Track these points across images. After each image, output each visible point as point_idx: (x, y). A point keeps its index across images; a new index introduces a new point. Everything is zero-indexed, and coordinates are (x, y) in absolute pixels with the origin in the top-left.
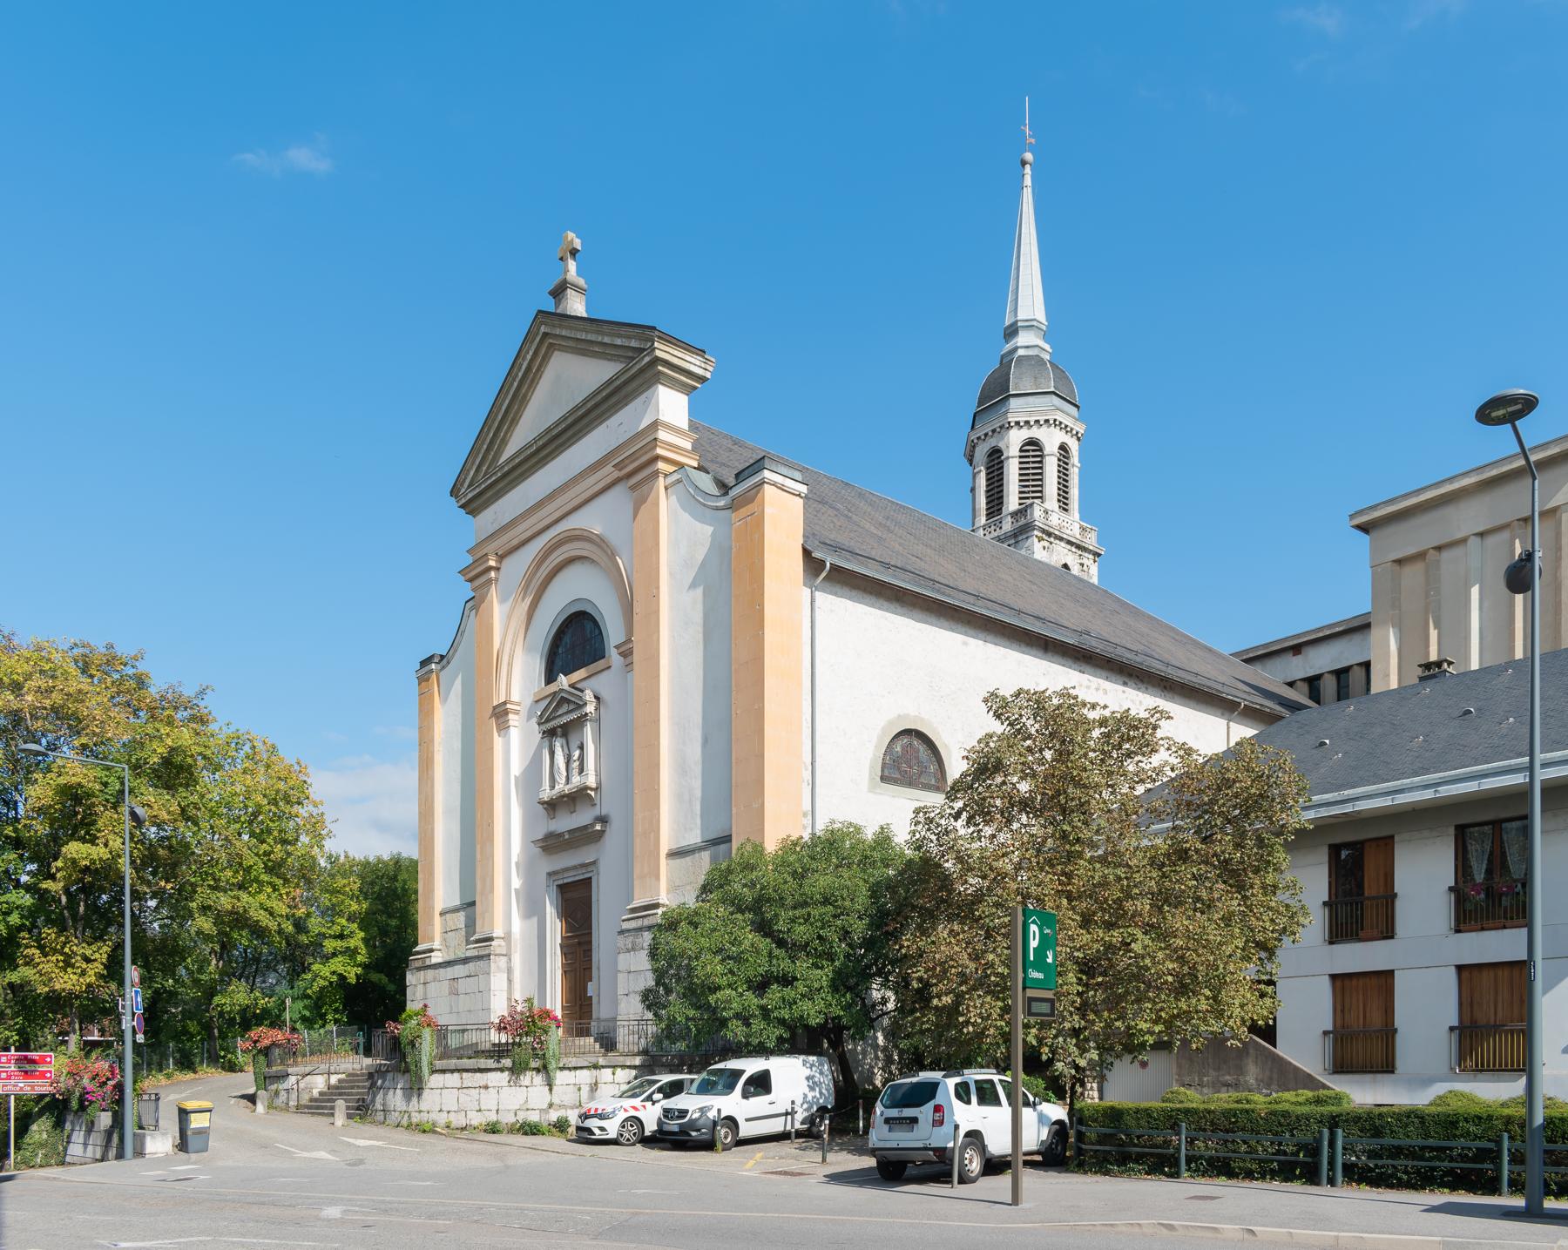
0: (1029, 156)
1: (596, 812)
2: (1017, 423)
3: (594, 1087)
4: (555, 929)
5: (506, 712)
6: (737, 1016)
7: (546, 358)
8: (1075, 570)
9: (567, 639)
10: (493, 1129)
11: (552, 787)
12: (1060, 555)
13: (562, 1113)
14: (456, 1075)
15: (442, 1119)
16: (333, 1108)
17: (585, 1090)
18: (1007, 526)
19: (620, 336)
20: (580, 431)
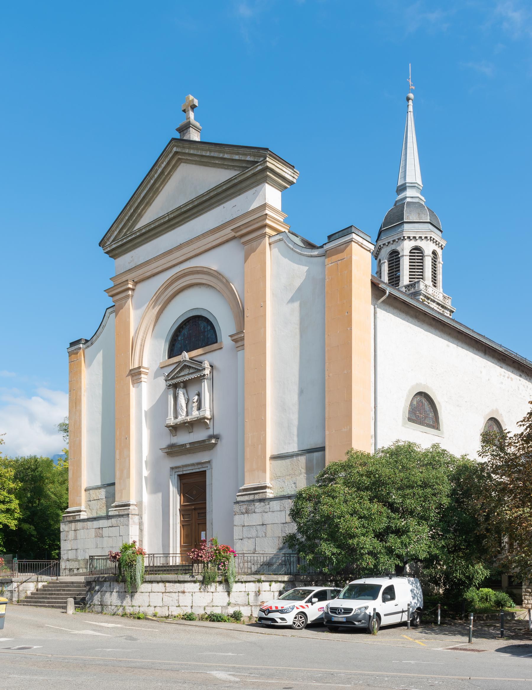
0: (411, 96)
1: (210, 432)
2: (409, 237)
3: (258, 593)
4: (175, 500)
5: (140, 373)
6: (370, 553)
7: (175, 167)
9: (185, 331)
10: (189, 617)
11: (176, 417)
13: (236, 609)
14: (161, 585)
15: (150, 611)
16: (66, 603)
17: (252, 595)
19: (238, 154)
20: (203, 209)
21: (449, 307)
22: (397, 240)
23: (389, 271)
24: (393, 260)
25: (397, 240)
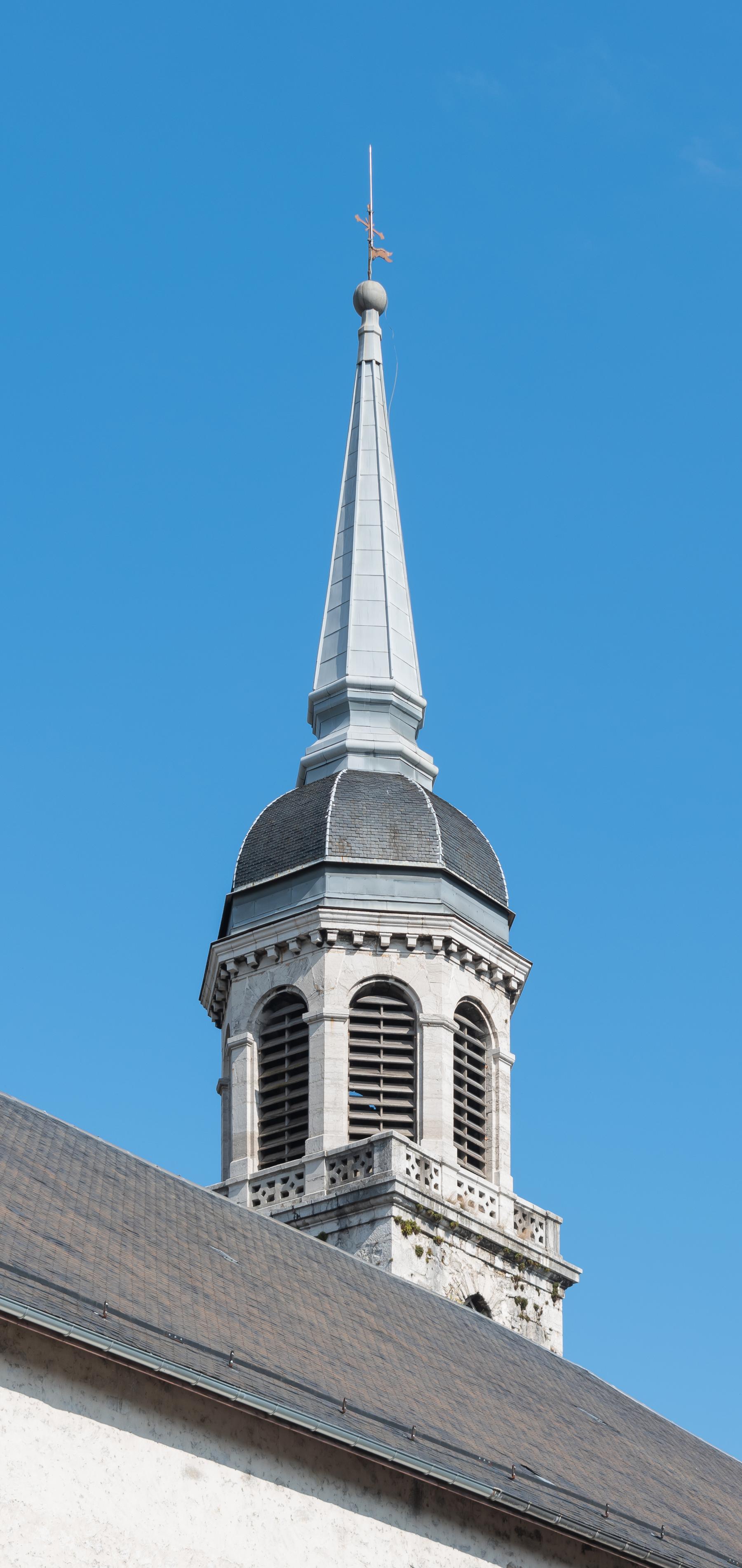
0: (375, 290)
2: (346, 936)
8: (503, 1314)
12: (462, 1272)
18: (318, 1186)
21: (545, 1263)
22: (293, 946)
23: (264, 1081)
24: (281, 1033)
25: (293, 946)
